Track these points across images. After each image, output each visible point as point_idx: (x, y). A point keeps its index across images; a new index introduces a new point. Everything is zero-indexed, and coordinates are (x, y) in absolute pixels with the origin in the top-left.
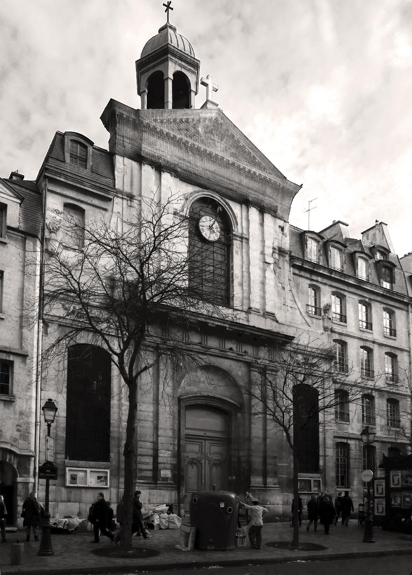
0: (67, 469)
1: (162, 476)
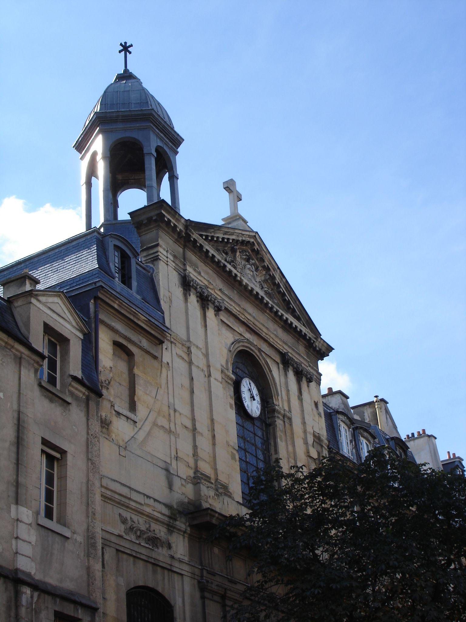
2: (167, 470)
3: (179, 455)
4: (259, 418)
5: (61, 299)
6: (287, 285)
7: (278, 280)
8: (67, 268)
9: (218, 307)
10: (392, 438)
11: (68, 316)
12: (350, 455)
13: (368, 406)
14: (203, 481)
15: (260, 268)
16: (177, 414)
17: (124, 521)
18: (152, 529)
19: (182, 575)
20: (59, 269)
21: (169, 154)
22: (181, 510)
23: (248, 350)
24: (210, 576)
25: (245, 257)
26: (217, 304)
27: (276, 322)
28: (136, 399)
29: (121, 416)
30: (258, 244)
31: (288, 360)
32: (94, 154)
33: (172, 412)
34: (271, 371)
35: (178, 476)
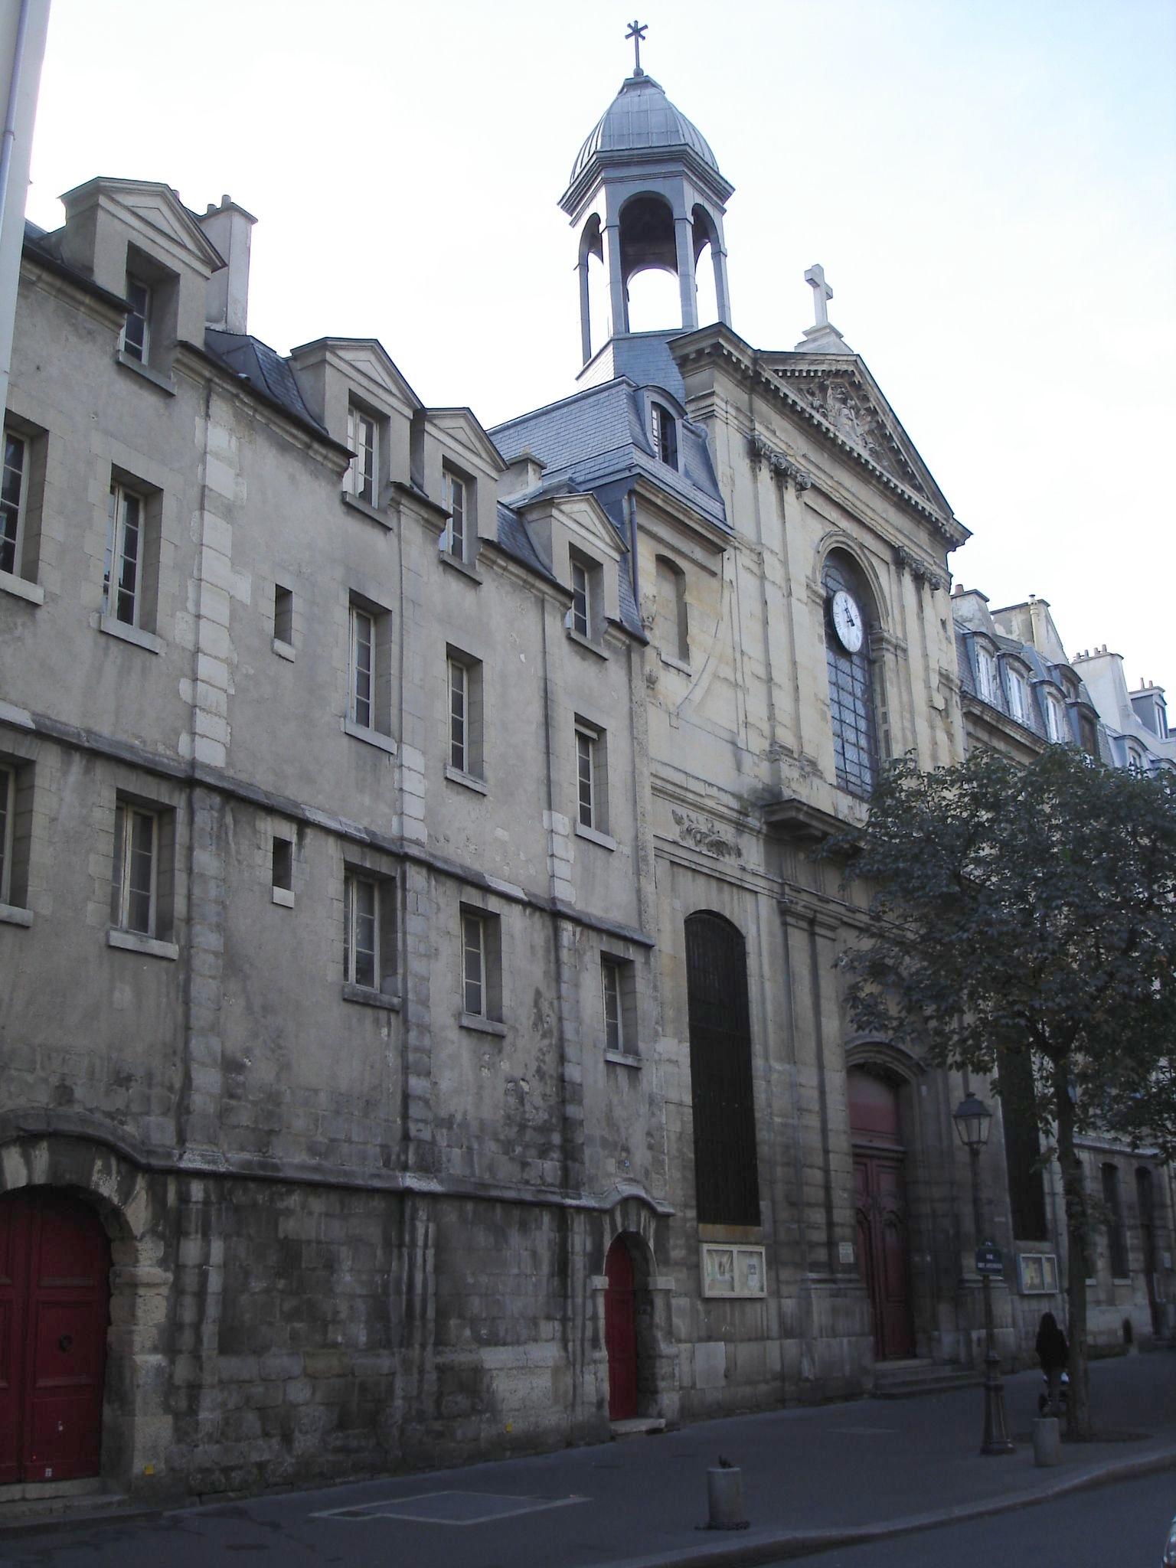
0: (705, 1247)
1: (841, 1261)
2: (734, 743)
3: (750, 719)
4: (860, 653)
5: (591, 505)
6: (905, 438)
7: (889, 430)
8: (582, 440)
9: (801, 485)
10: (1057, 666)
11: (599, 529)
12: (992, 699)
13: (1018, 610)
14: (783, 756)
15: (863, 412)
16: (746, 659)
17: (679, 821)
18: (715, 829)
19: (756, 892)
20: (570, 440)
21: (712, 214)
22: (753, 800)
23: (845, 547)
24: (794, 894)
25: (840, 396)
26: (799, 479)
27: (885, 497)
28: (689, 640)
29: (670, 668)
30: (861, 372)
31: (903, 559)
32: (595, 219)
33: (738, 656)
34: (877, 577)
35: (747, 751)
